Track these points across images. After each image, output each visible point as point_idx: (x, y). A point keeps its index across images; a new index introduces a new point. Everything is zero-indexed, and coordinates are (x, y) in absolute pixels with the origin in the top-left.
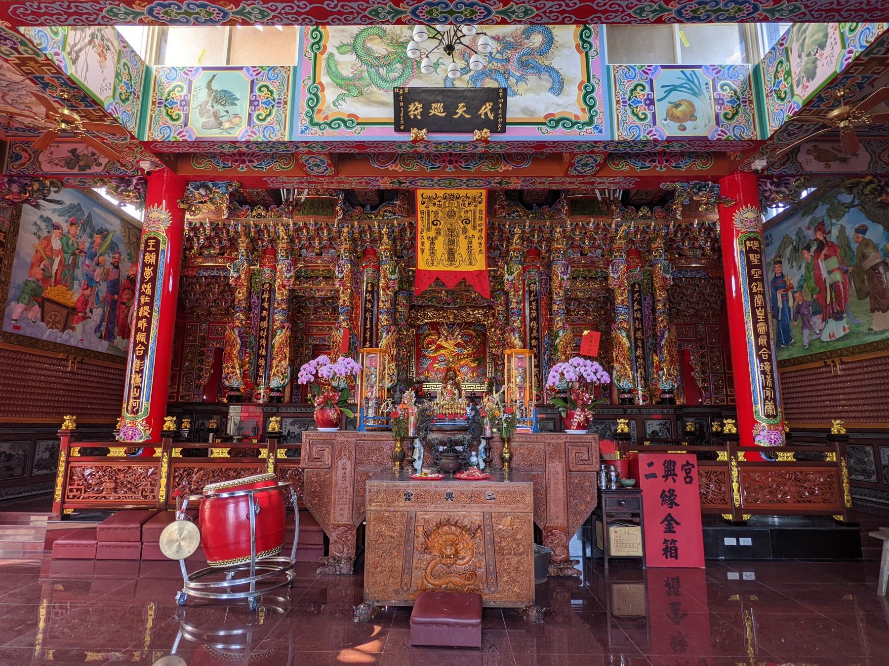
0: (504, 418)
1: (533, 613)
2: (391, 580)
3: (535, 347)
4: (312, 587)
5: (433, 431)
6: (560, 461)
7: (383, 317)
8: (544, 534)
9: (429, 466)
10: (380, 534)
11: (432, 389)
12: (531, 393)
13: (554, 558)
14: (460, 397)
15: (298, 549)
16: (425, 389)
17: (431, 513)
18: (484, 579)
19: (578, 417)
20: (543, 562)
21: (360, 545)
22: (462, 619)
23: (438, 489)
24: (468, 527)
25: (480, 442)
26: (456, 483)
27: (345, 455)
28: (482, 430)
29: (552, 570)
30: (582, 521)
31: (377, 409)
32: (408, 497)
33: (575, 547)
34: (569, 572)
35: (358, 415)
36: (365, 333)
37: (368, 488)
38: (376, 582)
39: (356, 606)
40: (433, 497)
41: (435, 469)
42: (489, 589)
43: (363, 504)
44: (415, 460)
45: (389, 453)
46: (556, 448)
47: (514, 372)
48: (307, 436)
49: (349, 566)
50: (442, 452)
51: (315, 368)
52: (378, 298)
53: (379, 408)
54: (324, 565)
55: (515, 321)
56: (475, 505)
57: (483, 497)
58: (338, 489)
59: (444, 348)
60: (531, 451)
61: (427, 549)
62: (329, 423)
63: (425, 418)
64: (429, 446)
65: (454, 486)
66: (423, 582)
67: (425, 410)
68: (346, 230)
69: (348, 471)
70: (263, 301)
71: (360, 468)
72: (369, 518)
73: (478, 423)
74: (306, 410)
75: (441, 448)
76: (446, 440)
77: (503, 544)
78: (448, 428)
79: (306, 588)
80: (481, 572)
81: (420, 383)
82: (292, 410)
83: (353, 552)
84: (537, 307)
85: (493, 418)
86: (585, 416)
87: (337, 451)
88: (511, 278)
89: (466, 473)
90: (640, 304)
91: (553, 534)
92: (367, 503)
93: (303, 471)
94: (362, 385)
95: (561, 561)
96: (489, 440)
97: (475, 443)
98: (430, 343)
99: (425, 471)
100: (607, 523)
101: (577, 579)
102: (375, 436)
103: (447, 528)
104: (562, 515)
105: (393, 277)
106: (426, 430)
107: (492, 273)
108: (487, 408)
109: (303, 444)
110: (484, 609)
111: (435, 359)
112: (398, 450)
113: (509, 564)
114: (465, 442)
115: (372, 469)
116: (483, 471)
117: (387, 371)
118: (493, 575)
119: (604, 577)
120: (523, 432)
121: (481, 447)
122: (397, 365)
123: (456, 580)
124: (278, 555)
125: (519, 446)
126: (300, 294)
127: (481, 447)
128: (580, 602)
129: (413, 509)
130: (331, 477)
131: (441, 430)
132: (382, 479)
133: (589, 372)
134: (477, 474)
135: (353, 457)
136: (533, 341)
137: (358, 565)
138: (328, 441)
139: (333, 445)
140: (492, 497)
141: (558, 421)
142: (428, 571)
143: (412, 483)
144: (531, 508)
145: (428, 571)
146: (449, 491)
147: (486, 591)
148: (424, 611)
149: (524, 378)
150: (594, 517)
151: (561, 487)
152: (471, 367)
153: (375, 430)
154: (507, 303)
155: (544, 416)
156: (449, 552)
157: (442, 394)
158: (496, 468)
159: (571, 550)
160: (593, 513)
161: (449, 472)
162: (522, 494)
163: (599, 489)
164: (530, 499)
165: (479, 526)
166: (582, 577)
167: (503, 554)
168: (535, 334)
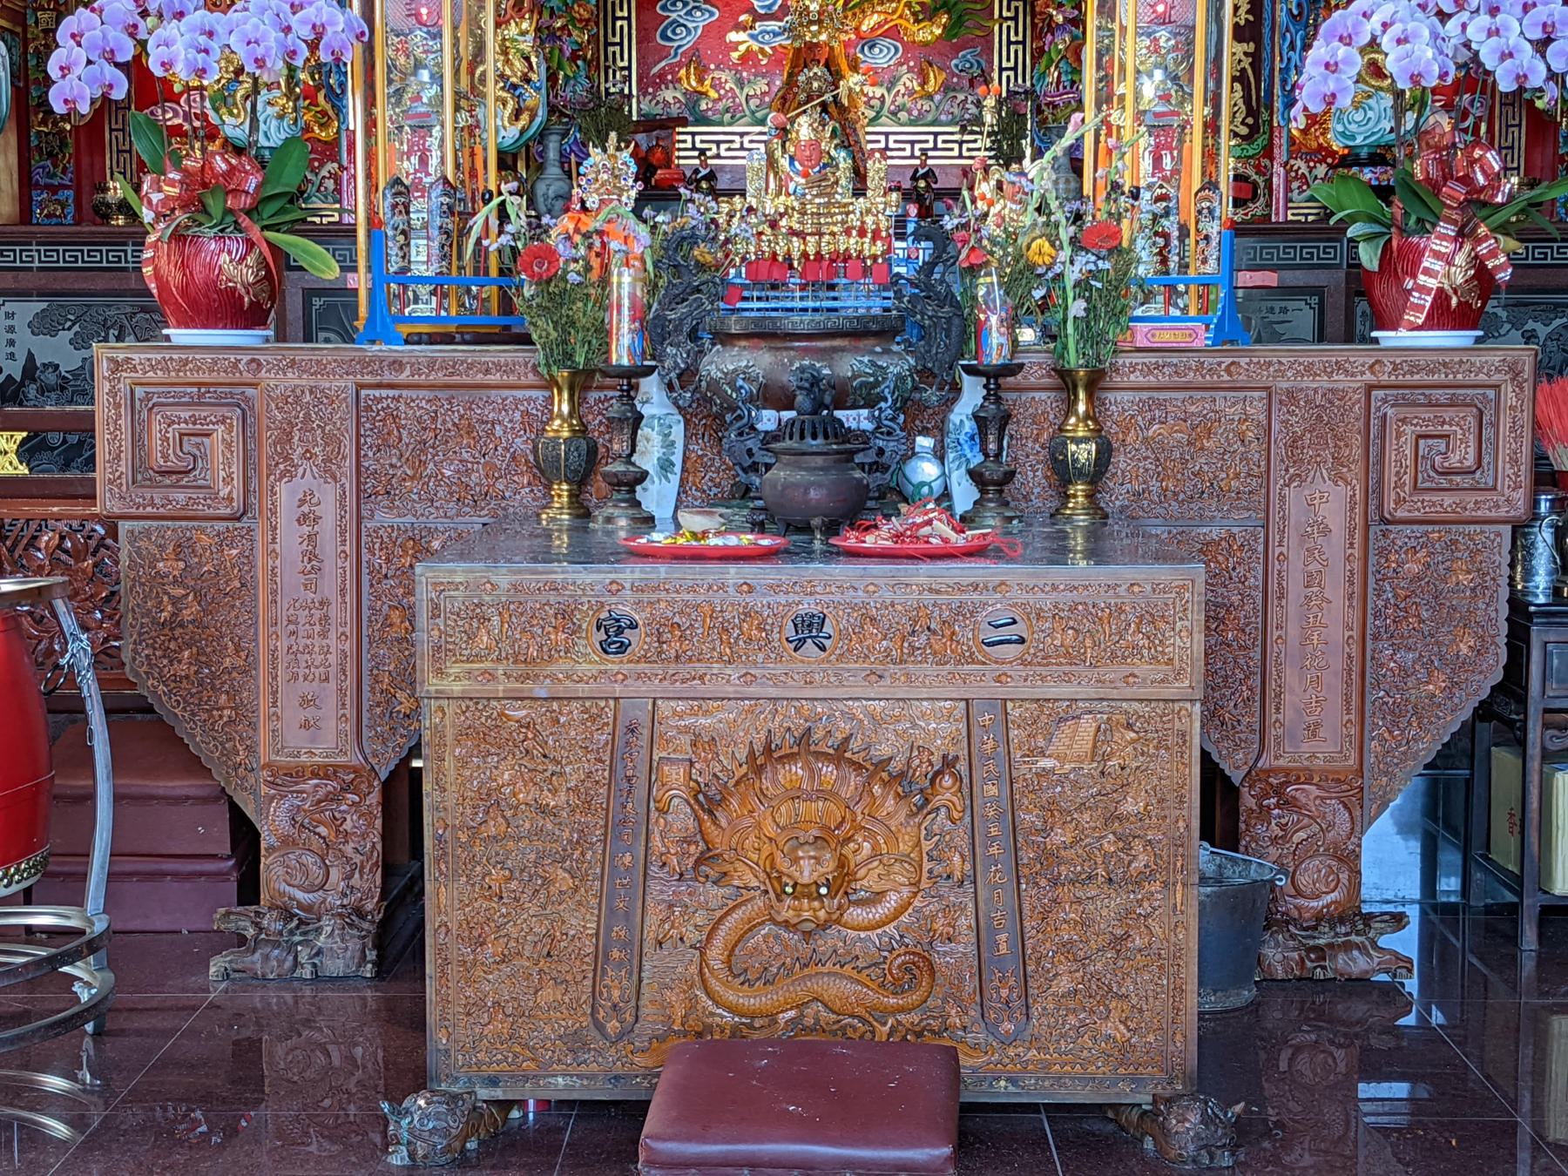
0: (1072, 275)
1: (1187, 1124)
2: (548, 994)
4: (192, 1033)
5: (725, 338)
6: (1337, 478)
8: (1248, 801)
9: (709, 503)
10: (490, 800)
11: (726, 160)
12: (1211, 156)
13: (1290, 905)
14: (859, 192)
15: (113, 877)
16: (686, 160)
17: (724, 706)
18: (970, 985)
19: (1441, 265)
20: (1241, 919)
21: (403, 857)
22: (868, 1143)
23: (758, 601)
24: (896, 766)
25: (956, 389)
26: (841, 570)
27: (308, 455)
28: (967, 330)
29: (1278, 956)
30: (1427, 747)
31: (453, 239)
32: (614, 636)
33: (1390, 863)
34: (1358, 964)
35: (360, 281)
37: (423, 595)
38: (480, 1004)
39: (396, 1099)
40: (735, 634)
41: (741, 515)
42: (991, 1028)
43: (407, 677)
44: (643, 476)
45: (521, 444)
46: (1324, 415)
47: (1131, 51)
48: (117, 366)
49: (354, 945)
50: (770, 438)
51: (132, 31)
53: (463, 232)
54: (242, 941)
56: (929, 668)
57: (965, 634)
58: (284, 608)
60: (1203, 429)
61: (707, 861)
62: (225, 308)
63: (682, 272)
64: (709, 412)
65: (824, 582)
66: (693, 1003)
67: (683, 241)
69: (328, 525)
71: (382, 518)
72: (438, 731)
73: (949, 298)
74: (104, 256)
75: (768, 420)
76: (789, 379)
77: (1059, 837)
78: (802, 323)
79: (167, 1034)
80: (954, 955)
81: (664, 125)
82: (35, 256)
83: (369, 883)
85: (1021, 275)
86: (1478, 263)
87: (269, 437)
89: (885, 529)
91: (1288, 804)
92: (424, 665)
93: (113, 532)
94: (370, 124)
95: (1319, 918)
96: (996, 377)
97: (931, 395)
99: (693, 521)
100: (1547, 756)
101: (1391, 994)
102: (452, 367)
103: (798, 769)
104: (1335, 719)
106: (693, 336)
108: (990, 228)
109: (102, 409)
110: (968, 1109)
112: (560, 429)
113: (1083, 924)
114: (886, 389)
115: (439, 519)
116: (967, 520)
117: (491, 63)
118: (1007, 975)
119: (1514, 986)
120: (1166, 337)
121: (962, 414)
122: (545, 35)
123: (841, 989)
124: (27, 897)
125: (1145, 407)
127: (962, 414)
128: (1400, 1089)
129: (643, 688)
130: (248, 559)
131: (766, 334)
132: (492, 556)
133: (1513, 38)
134: (942, 531)
135: (349, 464)
137: (397, 938)
138: (225, 393)
140: (1005, 633)
141: (1337, 300)
142: (716, 954)
143: (632, 573)
144: (1189, 683)
145: (716, 954)
146: (807, 606)
147: (979, 1035)
148: (701, 1112)
149: (1179, 81)
150: (1485, 730)
151: (1335, 590)
152: (910, 46)
153: (447, 339)
155: (1271, 279)
156: (806, 872)
157: (772, 163)
158: (1045, 494)
159: (1369, 876)
160: (1484, 712)
161: (806, 529)
162: (1151, 618)
163: (1519, 607)
164: (1187, 641)
165: (948, 763)
166: (1412, 985)
167: (1055, 882)
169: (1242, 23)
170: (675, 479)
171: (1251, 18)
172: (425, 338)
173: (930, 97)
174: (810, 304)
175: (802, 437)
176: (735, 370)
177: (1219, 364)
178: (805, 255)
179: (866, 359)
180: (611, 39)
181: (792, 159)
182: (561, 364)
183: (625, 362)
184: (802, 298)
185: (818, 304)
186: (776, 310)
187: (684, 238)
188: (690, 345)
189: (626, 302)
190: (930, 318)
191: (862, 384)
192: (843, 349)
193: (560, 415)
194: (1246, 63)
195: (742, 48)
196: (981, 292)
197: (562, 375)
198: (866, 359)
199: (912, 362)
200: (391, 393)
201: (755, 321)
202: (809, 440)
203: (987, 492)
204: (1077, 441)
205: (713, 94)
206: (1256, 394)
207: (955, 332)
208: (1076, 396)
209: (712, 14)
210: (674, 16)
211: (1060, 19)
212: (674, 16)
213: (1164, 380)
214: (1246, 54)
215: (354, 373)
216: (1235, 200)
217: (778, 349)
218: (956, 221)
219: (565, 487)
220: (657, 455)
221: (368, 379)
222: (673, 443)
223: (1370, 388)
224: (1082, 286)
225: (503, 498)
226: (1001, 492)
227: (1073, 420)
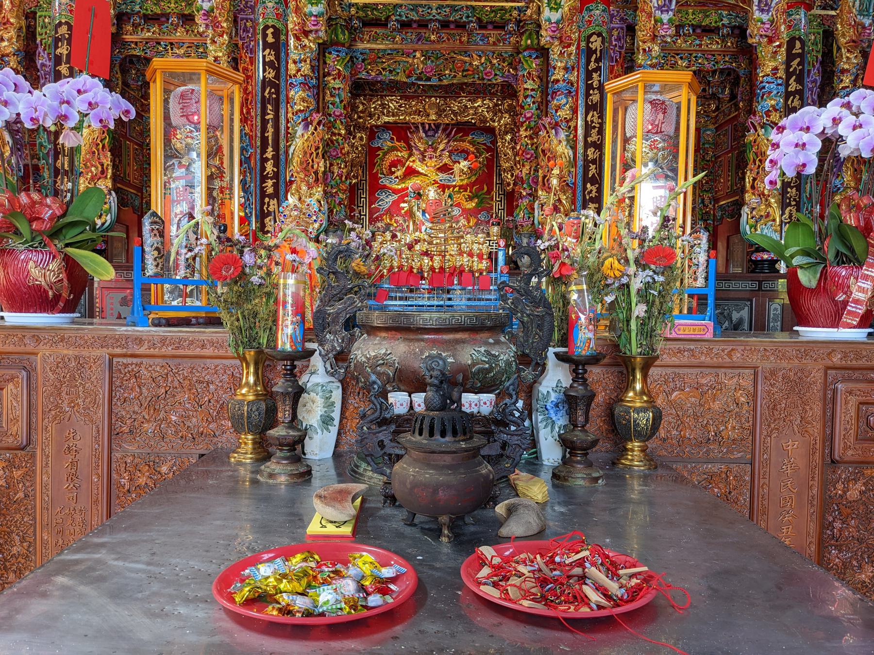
0: (636, 285)
3: (594, 162)
5: (372, 330)
7: (297, 94)
36: (264, 129)
52: (287, 55)
70: (58, 60)
73: (542, 301)
76: (418, 365)
78: (431, 318)
88: (555, 16)
90: (800, 80)
98: (394, 164)
102: (179, 343)
107: (515, 13)
112: (246, 394)
126: (137, 52)
131: (402, 328)
136: (590, 151)
139: (30, 373)
152: (464, 210)
154: (546, 67)
170: (334, 430)
172: (164, 321)
173: (471, 227)
174: (436, 303)
175: (431, 434)
176: (375, 357)
177: (723, 351)
178: (432, 269)
179: (482, 349)
181: (424, 212)
182: (249, 345)
183: (288, 347)
184: (429, 299)
185: (442, 303)
186: (412, 306)
187: (340, 252)
188: (344, 333)
189: (290, 300)
190: (528, 315)
191: (481, 370)
192: (463, 341)
193: (247, 383)
196: (574, 297)
197: (250, 354)
198: (482, 349)
199: (514, 349)
200: (135, 360)
201: (399, 315)
202: (437, 437)
203: (576, 455)
204: (638, 410)
205: (395, 225)
206: (747, 371)
207: (546, 327)
208: (634, 377)
211: (525, 194)
213: (685, 361)
215: (107, 346)
217: (411, 340)
218: (547, 244)
219: (250, 437)
220: (320, 413)
221: (118, 351)
222: (333, 404)
223: (828, 368)
224: (643, 295)
225: (215, 435)
226: (586, 454)
227: (631, 394)
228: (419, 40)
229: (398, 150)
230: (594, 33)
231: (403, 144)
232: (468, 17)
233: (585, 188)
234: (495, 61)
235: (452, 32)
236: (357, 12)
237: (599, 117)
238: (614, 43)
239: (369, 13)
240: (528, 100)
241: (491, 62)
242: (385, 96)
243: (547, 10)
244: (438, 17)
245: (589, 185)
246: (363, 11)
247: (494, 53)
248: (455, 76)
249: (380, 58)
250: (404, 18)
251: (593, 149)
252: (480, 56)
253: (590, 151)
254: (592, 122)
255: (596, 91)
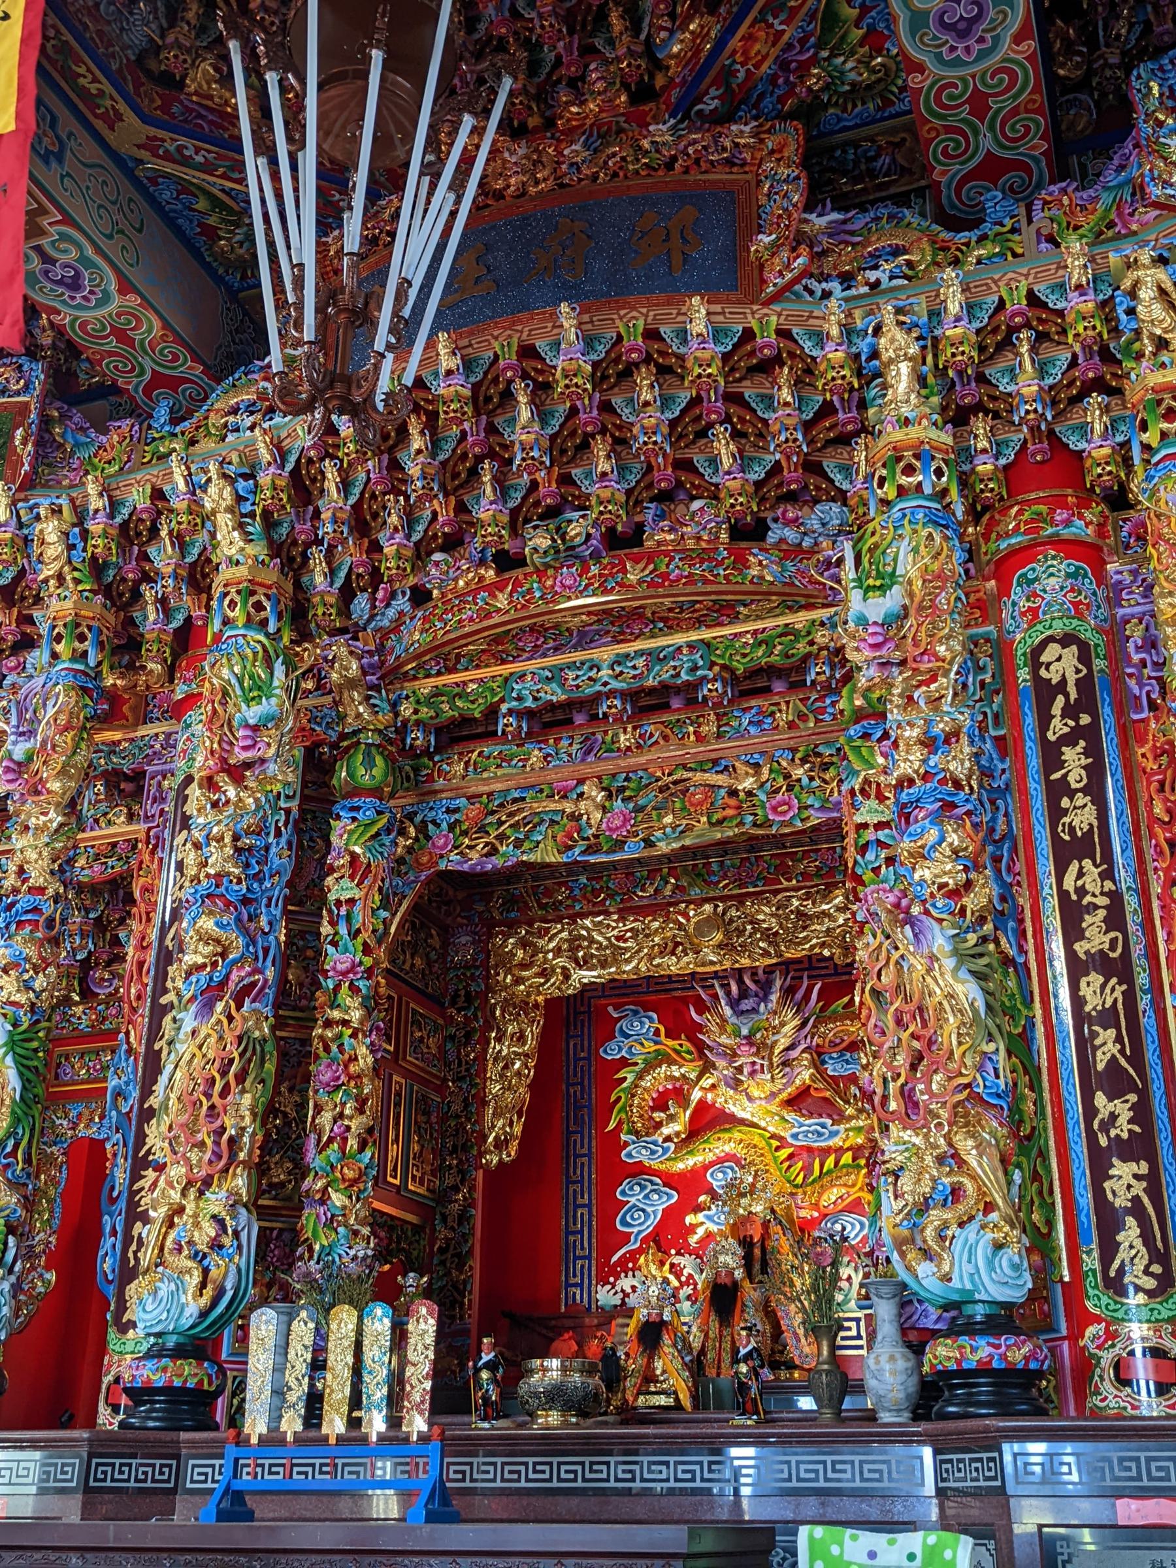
3: (1108, 1018)
55: (921, 856)
59: (732, 1121)
68: (50, 530)
84: (1095, 772)
105: (253, 714)
111: (690, 1188)
136: (1091, 984)
168: (1096, 938)
169: (1125, 1135)
171: (1137, 1129)
180: (572, 1228)
194: (1139, 1188)
195: (700, 1231)
209: (669, 1196)
210: (633, 1200)
212: (633, 1200)
214: (1136, 1177)
216: (1157, 1384)
228: (588, 752)
229: (672, 1062)
230: (1051, 639)
231: (687, 1045)
232: (695, 668)
233: (1090, 1111)
234: (799, 772)
235: (673, 718)
236: (416, 712)
237: (1104, 876)
238: (1136, 658)
239: (446, 707)
240: (870, 856)
241: (787, 776)
242: (583, 916)
243: (855, 596)
244: (615, 684)
245: (1100, 1099)
246: (429, 704)
247: (794, 750)
248: (689, 828)
249: (493, 813)
250: (529, 703)
251: (1096, 979)
252: (757, 766)
253: (1091, 984)
254: (1081, 891)
255: (1080, 799)
